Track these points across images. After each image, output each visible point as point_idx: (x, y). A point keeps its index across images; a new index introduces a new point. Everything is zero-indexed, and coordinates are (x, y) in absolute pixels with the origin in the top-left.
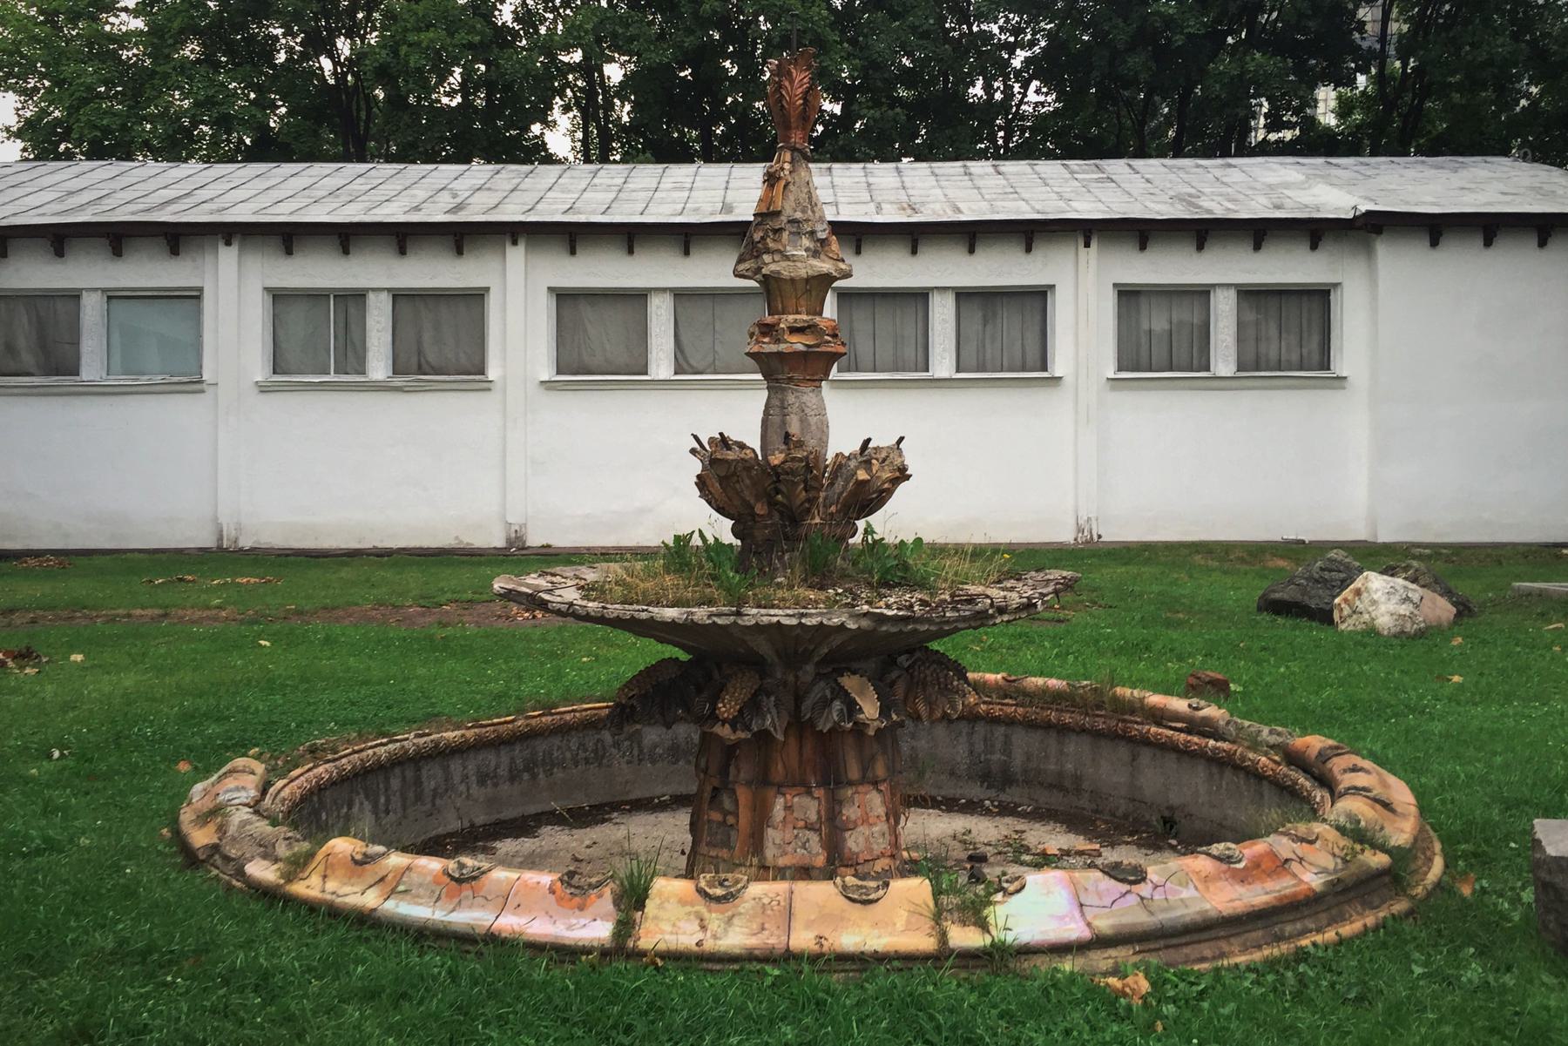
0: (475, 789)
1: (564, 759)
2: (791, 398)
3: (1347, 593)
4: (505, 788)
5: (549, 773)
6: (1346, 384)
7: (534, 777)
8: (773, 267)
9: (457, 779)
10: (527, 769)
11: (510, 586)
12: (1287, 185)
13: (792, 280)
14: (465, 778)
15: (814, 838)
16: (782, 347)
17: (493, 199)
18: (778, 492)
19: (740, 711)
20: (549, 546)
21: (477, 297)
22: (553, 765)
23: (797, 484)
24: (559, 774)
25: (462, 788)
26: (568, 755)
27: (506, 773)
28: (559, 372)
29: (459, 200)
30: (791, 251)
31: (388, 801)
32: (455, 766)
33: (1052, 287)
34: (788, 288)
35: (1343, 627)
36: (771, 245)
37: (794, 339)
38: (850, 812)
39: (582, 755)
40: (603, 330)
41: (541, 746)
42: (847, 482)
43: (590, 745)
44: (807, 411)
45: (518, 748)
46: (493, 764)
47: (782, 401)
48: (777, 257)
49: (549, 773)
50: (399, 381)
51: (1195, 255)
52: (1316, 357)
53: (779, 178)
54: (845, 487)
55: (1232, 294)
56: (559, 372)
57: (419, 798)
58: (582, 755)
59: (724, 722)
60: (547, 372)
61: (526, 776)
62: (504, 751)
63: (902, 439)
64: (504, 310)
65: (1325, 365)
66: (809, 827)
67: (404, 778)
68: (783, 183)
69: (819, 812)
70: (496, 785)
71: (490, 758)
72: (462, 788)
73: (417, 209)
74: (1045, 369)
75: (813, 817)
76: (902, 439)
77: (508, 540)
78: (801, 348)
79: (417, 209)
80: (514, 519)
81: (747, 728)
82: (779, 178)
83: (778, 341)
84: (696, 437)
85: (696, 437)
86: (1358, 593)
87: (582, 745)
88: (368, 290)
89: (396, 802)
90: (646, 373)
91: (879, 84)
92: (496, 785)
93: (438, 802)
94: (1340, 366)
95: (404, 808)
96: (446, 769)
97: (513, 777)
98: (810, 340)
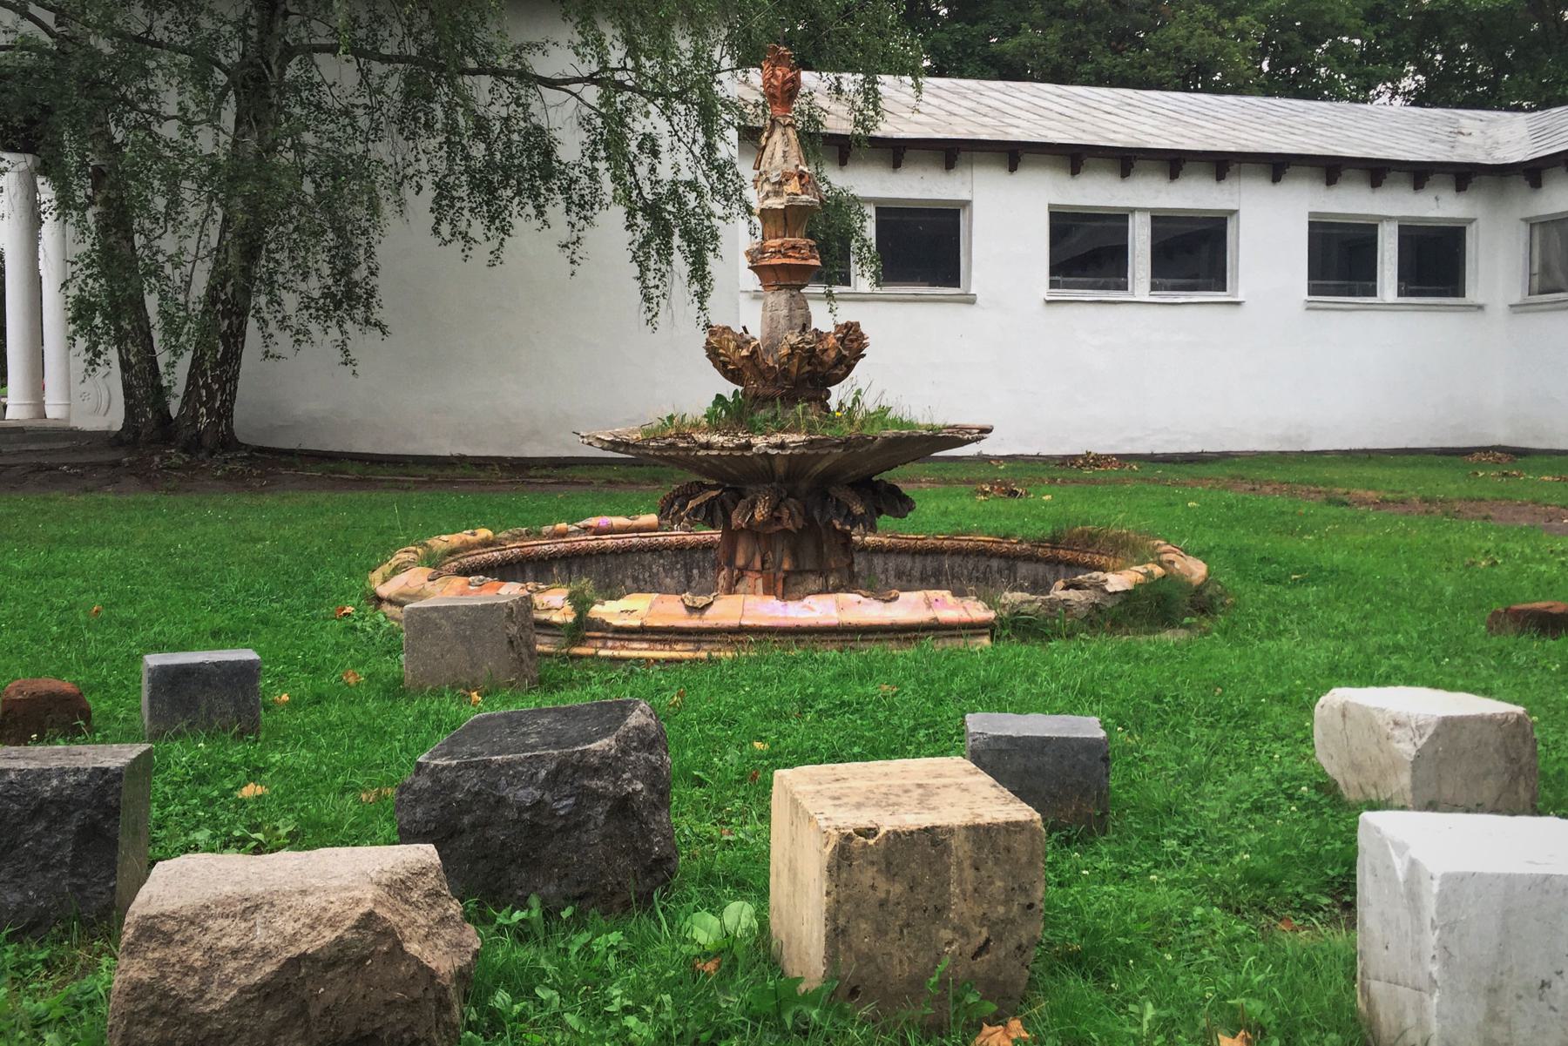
6: (1487, 309)
9: (879, 570)
14: (885, 571)
25: (882, 577)
32: (878, 561)
33: (1234, 212)
39: (975, 574)
43: (982, 568)
51: (1324, 186)
55: (1147, 219)
56: (1400, 294)
58: (975, 574)
62: (918, 559)
64: (970, 226)
71: (907, 562)
87: (976, 568)
88: (1133, 210)
90: (1375, 295)
91: (156, 183)
96: (870, 562)
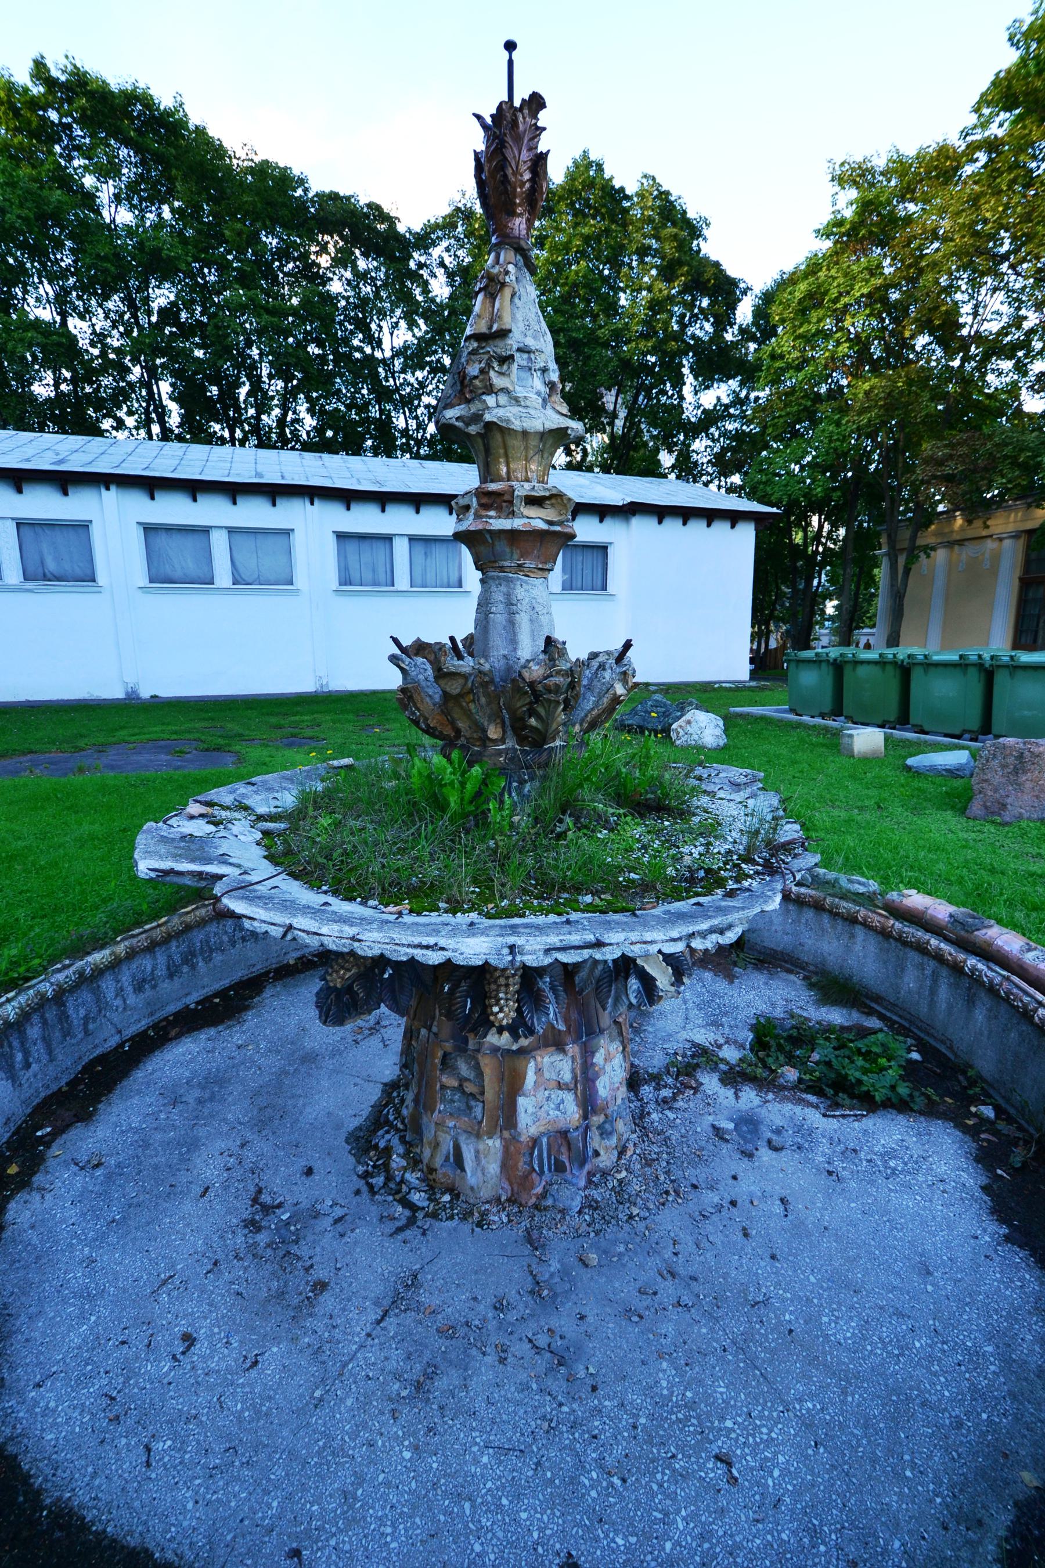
0: (132, 1000)
1: (222, 943)
2: (520, 592)
3: (681, 722)
4: (166, 986)
5: (208, 960)
7: (193, 967)
8: (501, 412)
9: (110, 995)
10: (186, 961)
11: (166, 865)
12: (581, 486)
13: (525, 433)
14: (120, 992)
15: (569, 1098)
16: (517, 523)
17: (89, 458)
18: (532, 713)
19: (519, 1011)
20: (156, 696)
21: (83, 527)
22: (211, 951)
23: (558, 703)
24: (218, 957)
25: (118, 1002)
26: (225, 938)
27: (164, 972)
28: (151, 582)
29: (60, 457)
30: (520, 392)
31: (26, 1054)
34: (515, 443)
35: (678, 742)
36: (498, 381)
37: (532, 511)
38: (599, 1058)
40: (180, 555)
41: (198, 937)
42: (600, 697)
44: (538, 608)
45: (174, 943)
46: (149, 968)
47: (508, 595)
48: (503, 399)
49: (208, 960)
50: (30, 585)
52: (599, 583)
53: (503, 285)
54: (596, 704)
56: (151, 582)
57: (67, 1033)
59: (500, 1030)
60: (144, 581)
61: (185, 969)
63: (628, 645)
65: (604, 588)
66: (560, 1086)
67: (45, 1022)
68: (507, 292)
69: (573, 1071)
70: (154, 987)
71: (146, 963)
72: (118, 1002)
73: (28, 460)
74: (460, 586)
75: (567, 1077)
76: (628, 645)
77: (127, 693)
78: (542, 525)
79: (28, 460)
80: (131, 680)
81: (531, 1031)
82: (503, 285)
83: (512, 514)
84: (396, 641)
85: (396, 641)
86: (689, 722)
89: (38, 1050)
92: (154, 987)
93: (91, 1026)
94: (611, 588)
95: (50, 1052)
97: (172, 973)
98: (550, 514)
